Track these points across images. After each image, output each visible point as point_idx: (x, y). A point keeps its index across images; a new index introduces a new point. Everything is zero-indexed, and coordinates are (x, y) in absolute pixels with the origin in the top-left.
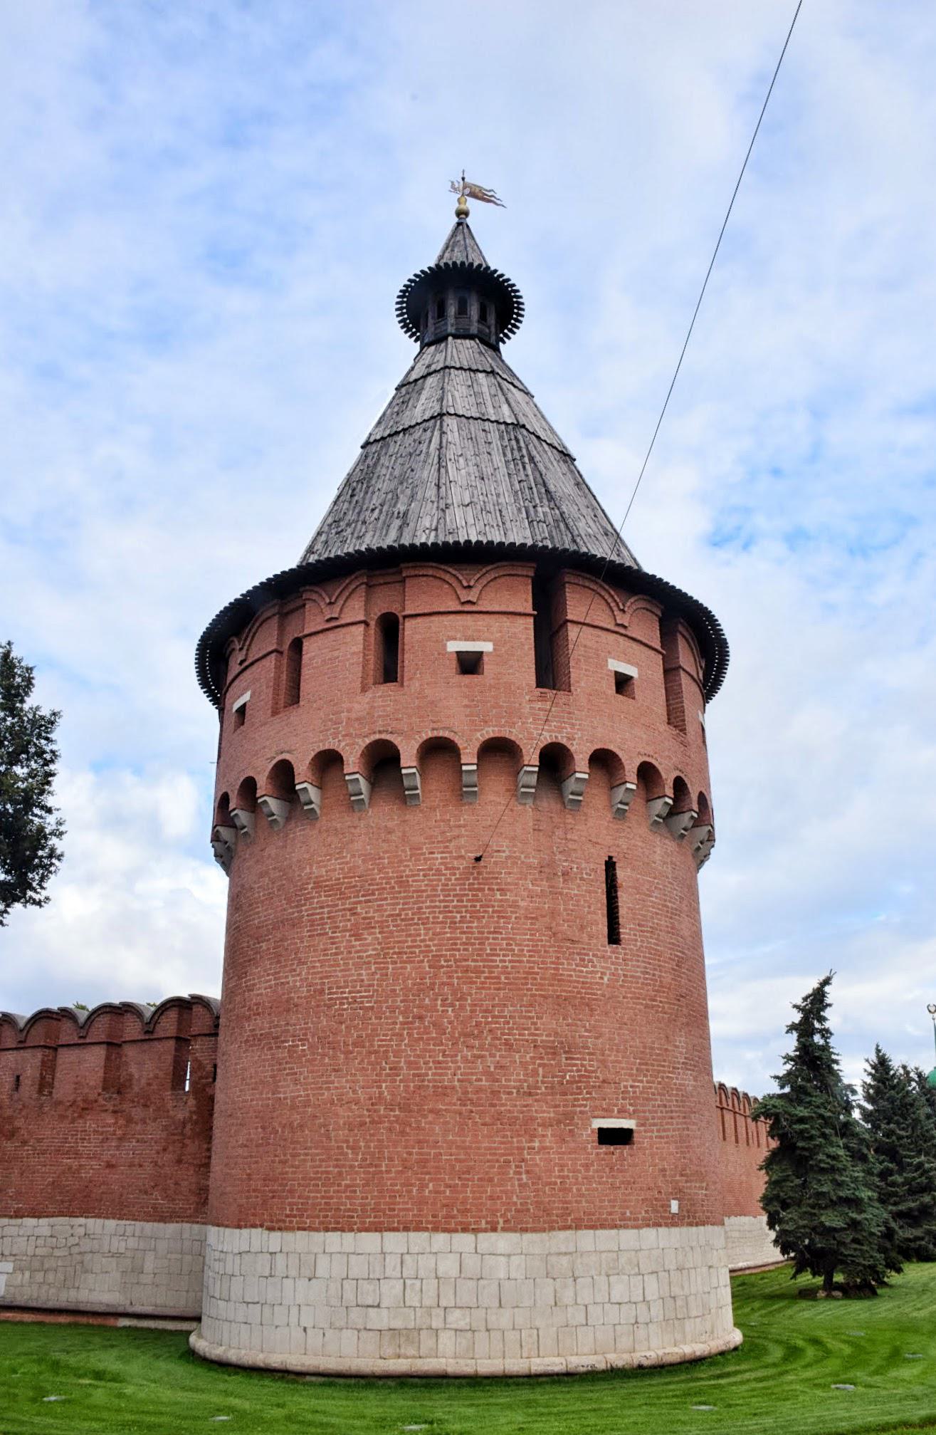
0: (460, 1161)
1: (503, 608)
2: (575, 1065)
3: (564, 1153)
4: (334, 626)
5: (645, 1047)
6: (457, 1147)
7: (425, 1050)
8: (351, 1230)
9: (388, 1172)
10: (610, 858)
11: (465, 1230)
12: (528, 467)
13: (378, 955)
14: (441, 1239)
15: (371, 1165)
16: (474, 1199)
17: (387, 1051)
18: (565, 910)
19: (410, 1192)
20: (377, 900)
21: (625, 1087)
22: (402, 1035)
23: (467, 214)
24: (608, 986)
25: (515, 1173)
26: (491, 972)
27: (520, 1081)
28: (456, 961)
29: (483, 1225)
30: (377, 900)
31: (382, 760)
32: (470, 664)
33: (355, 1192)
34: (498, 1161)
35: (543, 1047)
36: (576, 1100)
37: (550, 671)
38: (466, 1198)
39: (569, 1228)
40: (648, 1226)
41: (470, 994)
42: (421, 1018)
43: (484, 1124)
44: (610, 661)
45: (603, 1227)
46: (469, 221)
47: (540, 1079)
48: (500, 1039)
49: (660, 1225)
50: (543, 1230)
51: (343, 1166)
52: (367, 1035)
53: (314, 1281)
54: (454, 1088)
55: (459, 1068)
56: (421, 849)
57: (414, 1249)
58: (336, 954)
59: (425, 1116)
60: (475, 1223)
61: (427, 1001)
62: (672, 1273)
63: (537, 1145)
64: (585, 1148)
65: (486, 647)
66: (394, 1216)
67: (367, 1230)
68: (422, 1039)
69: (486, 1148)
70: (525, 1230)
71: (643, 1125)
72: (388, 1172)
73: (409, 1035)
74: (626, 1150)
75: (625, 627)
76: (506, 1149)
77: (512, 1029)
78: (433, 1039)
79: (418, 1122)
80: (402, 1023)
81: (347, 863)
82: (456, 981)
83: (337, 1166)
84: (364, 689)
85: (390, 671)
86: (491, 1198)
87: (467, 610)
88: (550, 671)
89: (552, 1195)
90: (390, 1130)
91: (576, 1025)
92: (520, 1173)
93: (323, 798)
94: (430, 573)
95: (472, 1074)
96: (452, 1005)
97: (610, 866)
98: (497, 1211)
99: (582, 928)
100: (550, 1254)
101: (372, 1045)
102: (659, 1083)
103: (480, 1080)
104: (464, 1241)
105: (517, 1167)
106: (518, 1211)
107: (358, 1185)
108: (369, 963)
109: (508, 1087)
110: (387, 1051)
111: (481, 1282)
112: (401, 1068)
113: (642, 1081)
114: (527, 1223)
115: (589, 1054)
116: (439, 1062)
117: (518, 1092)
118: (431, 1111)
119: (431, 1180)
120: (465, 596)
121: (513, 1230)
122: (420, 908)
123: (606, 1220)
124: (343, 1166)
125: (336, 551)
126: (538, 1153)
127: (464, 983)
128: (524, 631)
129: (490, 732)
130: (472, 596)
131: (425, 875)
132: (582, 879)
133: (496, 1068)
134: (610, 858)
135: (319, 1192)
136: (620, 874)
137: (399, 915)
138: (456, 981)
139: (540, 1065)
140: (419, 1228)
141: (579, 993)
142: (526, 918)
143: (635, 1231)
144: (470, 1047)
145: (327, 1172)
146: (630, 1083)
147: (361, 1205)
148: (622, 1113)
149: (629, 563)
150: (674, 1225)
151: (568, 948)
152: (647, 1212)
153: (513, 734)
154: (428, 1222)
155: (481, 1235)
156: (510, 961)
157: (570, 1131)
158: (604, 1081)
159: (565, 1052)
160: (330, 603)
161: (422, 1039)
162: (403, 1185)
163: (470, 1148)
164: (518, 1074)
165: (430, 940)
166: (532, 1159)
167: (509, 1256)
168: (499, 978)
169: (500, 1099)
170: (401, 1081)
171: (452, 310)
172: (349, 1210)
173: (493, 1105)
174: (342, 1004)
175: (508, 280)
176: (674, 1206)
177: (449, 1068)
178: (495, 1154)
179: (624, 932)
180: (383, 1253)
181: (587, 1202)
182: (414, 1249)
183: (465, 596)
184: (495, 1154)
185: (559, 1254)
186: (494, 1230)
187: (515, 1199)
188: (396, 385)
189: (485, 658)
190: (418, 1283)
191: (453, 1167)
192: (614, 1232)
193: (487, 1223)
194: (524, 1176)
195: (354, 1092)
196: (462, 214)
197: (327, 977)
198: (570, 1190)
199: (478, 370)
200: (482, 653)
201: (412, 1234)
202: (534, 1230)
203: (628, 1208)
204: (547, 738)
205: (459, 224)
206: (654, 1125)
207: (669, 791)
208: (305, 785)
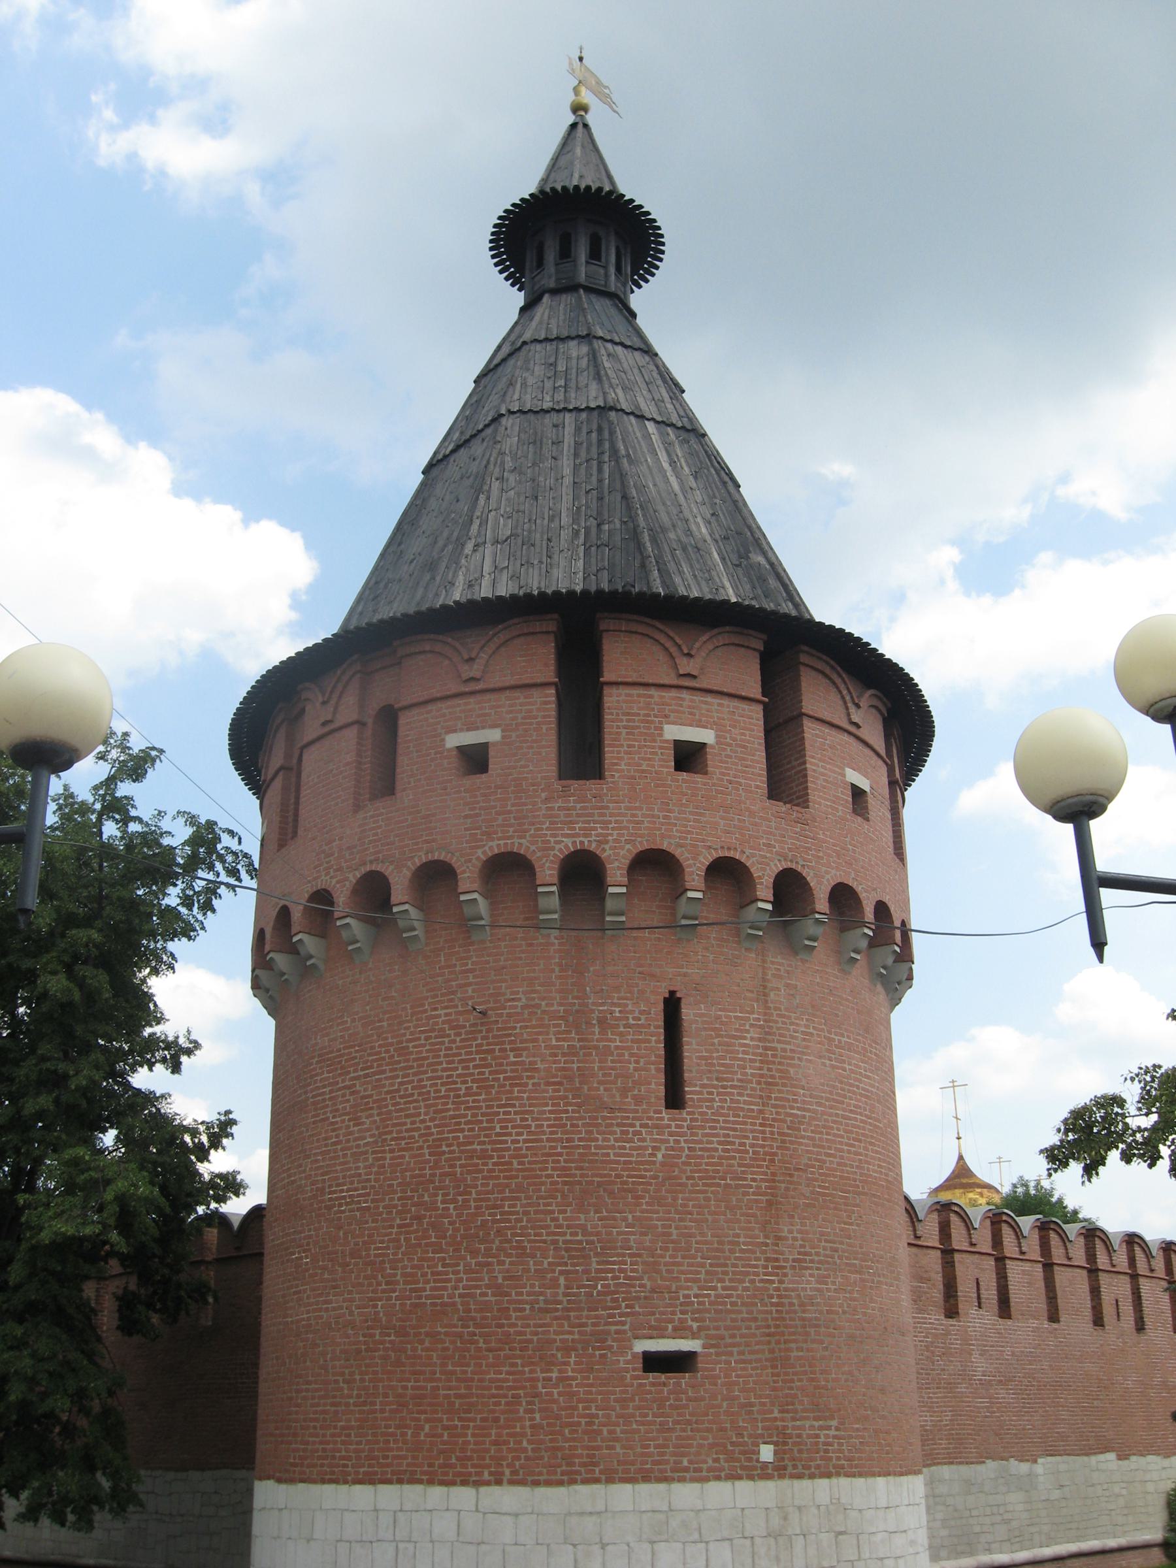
0: (457, 1396)
1: (510, 680)
2: (612, 1271)
3: (592, 1385)
4: (330, 730)
5: (720, 1243)
6: (458, 1380)
7: (422, 1259)
8: (346, 1482)
9: (382, 1411)
10: (672, 993)
11: (464, 1483)
12: (606, 467)
13: (376, 1142)
14: (437, 1493)
15: (364, 1404)
16: (476, 1443)
17: (383, 1262)
18: (601, 1068)
19: (404, 1434)
20: (375, 1074)
21: (687, 1296)
22: (398, 1240)
23: (585, 109)
24: (663, 1164)
25: (526, 1411)
26: (499, 1157)
27: (534, 1294)
28: (459, 1144)
29: (486, 1476)
30: (375, 1074)
31: (374, 892)
32: (475, 760)
33: (349, 1435)
34: (505, 1396)
35: (567, 1250)
36: (612, 1316)
37: (785, 780)
38: (466, 1443)
39: (597, 1481)
40: (718, 1478)
41: (476, 1186)
42: (419, 1218)
43: (490, 1350)
44: (666, 727)
45: (646, 1479)
46: (590, 118)
47: (561, 1290)
48: (510, 1241)
49: (740, 1478)
50: (560, 1483)
51: (339, 1404)
52: (364, 1243)
53: (312, 1542)
54: (454, 1304)
55: (460, 1280)
56: (423, 1005)
57: (408, 1506)
58: (335, 1143)
59: (422, 1342)
60: (477, 1474)
61: (426, 1198)
62: (758, 1541)
63: (554, 1375)
64: (623, 1378)
65: (492, 735)
66: (388, 1465)
67: (360, 1482)
68: (420, 1245)
69: (491, 1381)
70: (536, 1483)
71: (713, 1346)
72: (382, 1411)
73: (407, 1240)
74: (685, 1379)
75: (858, 726)
76: (514, 1381)
77: (525, 1228)
78: (432, 1244)
79: (414, 1349)
80: (399, 1226)
81: (348, 1029)
82: (458, 1170)
83: (333, 1404)
84: (357, 808)
85: (386, 783)
86: (495, 1443)
87: (472, 690)
88: (785, 780)
89: (574, 1440)
90: (385, 1358)
91: (615, 1219)
92: (532, 1411)
93: (493, 906)
94: (428, 648)
95: (477, 1287)
96: (454, 1201)
97: (672, 1005)
98: (503, 1458)
99: (624, 1092)
100: (570, 1514)
101: (368, 1256)
102: (746, 1289)
103: (485, 1294)
104: (463, 1496)
105: (528, 1403)
106: (527, 1459)
107: (351, 1428)
108: (366, 1153)
109: (520, 1302)
110: (383, 1262)
111: (483, 1547)
112: (397, 1283)
113: (714, 1288)
114: (540, 1474)
115: (631, 1255)
116: (439, 1273)
117: (532, 1309)
118: (427, 1334)
119: (427, 1420)
120: (468, 671)
121: (522, 1483)
122: (421, 1080)
123: (651, 1471)
124: (339, 1404)
125: (386, 612)
126: (556, 1386)
127: (469, 1172)
128: (543, 707)
129: (494, 846)
130: (475, 670)
131: (426, 1039)
132: (627, 1026)
133: (504, 1278)
134: (672, 993)
135: (317, 1435)
136: (688, 1013)
137: (398, 1091)
138: (458, 1170)
139: (561, 1272)
140: (413, 1481)
141: (617, 1176)
142: (548, 1084)
143: (697, 1486)
144: (474, 1253)
145: (324, 1412)
146: (696, 1291)
147: (356, 1451)
148: (681, 1331)
149: (807, 616)
150: (768, 1477)
151: (604, 1118)
152: (716, 1460)
153: (522, 845)
154: (423, 1473)
155: (483, 1489)
156: (525, 1141)
157: (601, 1356)
158: (653, 1291)
159: (597, 1255)
160: (324, 703)
161: (420, 1245)
162: (398, 1427)
163: (472, 1380)
164: (532, 1286)
165: (432, 1120)
166: (547, 1394)
167: (517, 1515)
168: (511, 1163)
169: (508, 1318)
170: (397, 1298)
171: (551, 256)
172: (343, 1458)
173: (501, 1326)
174: (340, 1205)
175: (648, 213)
176: (767, 1453)
177: (449, 1281)
178: (501, 1388)
179: (691, 1091)
180: (376, 1510)
181: (623, 1447)
182: (408, 1506)
183: (468, 671)
184: (501, 1388)
185: (582, 1514)
186: (499, 1482)
187: (525, 1444)
188: (474, 377)
189: (492, 753)
190: (411, 1546)
191: (452, 1404)
192: (662, 1487)
193: (491, 1474)
194: (537, 1416)
195: (351, 1313)
196: (579, 108)
197: (326, 1173)
198: (599, 1432)
199: (569, 338)
200: (487, 743)
201: (407, 1488)
202: (548, 1483)
203: (683, 1455)
204: (567, 844)
205: (574, 126)
206: (734, 1345)
207: (869, 915)
208: (475, 896)
